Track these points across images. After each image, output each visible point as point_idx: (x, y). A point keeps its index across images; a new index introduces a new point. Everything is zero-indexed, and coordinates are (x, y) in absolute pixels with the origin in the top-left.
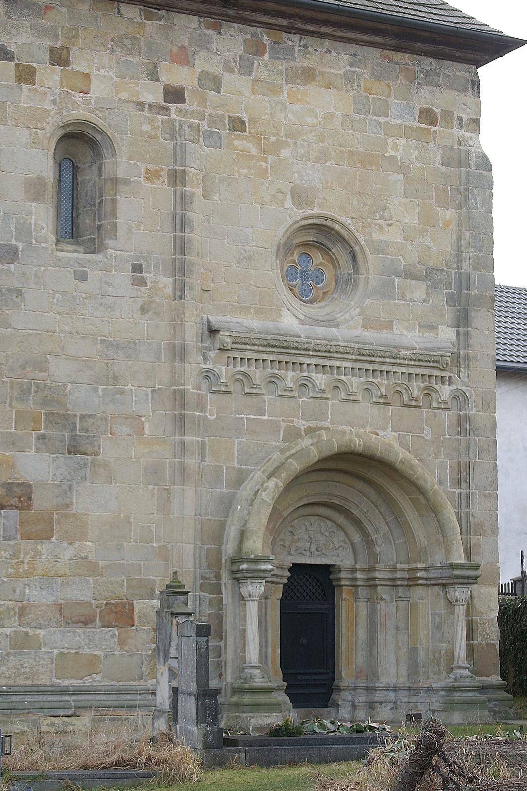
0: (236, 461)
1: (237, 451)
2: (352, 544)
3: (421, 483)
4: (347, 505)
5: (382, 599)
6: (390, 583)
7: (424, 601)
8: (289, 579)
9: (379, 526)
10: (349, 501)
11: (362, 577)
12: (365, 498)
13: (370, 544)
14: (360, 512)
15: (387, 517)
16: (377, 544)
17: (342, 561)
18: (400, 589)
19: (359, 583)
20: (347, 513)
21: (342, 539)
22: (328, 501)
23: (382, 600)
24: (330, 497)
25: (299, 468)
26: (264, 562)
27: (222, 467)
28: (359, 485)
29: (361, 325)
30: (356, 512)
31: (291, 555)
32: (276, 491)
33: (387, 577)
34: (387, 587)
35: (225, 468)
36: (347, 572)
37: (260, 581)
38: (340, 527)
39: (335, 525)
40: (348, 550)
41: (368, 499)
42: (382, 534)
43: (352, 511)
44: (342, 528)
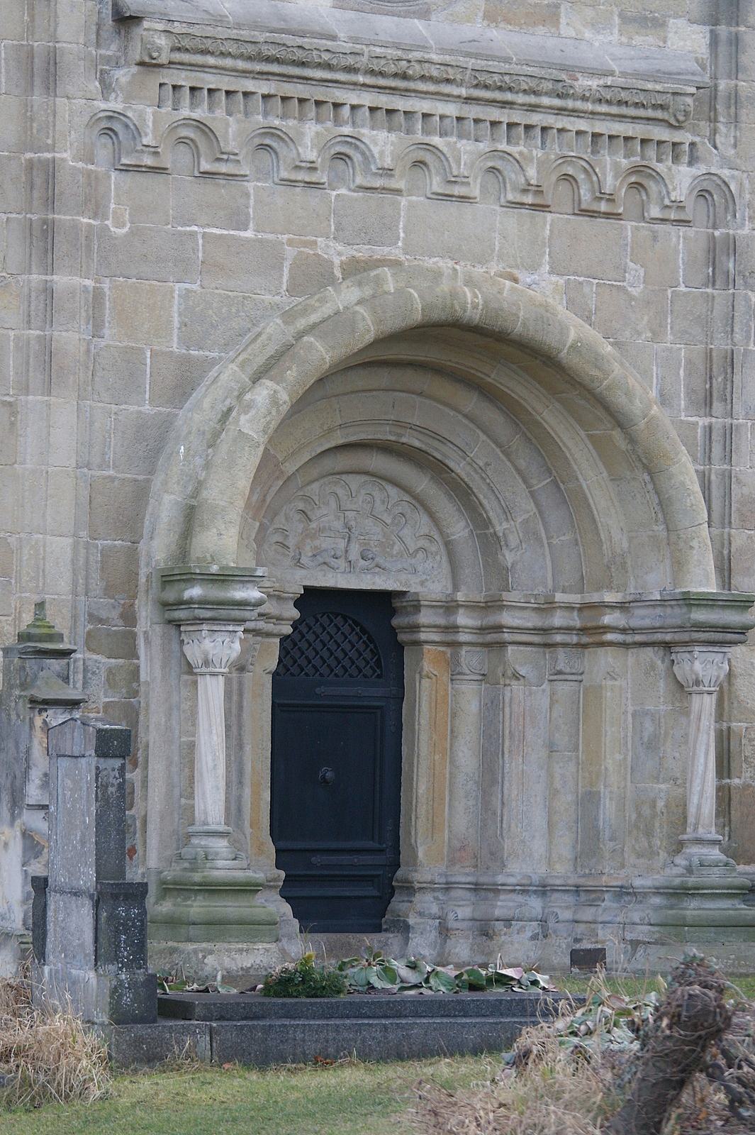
0: (175, 339)
1: (180, 315)
2: (447, 544)
4: (437, 449)
5: (516, 676)
9: (514, 504)
10: (444, 440)
13: (489, 543)
14: (468, 468)
18: (561, 652)
19: (463, 637)
21: (425, 530)
22: (393, 438)
27: (141, 351)
28: (470, 402)
29: (481, 14)
30: (460, 468)
33: (530, 625)
35: (148, 354)
37: (231, 628)
38: (420, 502)
41: (488, 436)
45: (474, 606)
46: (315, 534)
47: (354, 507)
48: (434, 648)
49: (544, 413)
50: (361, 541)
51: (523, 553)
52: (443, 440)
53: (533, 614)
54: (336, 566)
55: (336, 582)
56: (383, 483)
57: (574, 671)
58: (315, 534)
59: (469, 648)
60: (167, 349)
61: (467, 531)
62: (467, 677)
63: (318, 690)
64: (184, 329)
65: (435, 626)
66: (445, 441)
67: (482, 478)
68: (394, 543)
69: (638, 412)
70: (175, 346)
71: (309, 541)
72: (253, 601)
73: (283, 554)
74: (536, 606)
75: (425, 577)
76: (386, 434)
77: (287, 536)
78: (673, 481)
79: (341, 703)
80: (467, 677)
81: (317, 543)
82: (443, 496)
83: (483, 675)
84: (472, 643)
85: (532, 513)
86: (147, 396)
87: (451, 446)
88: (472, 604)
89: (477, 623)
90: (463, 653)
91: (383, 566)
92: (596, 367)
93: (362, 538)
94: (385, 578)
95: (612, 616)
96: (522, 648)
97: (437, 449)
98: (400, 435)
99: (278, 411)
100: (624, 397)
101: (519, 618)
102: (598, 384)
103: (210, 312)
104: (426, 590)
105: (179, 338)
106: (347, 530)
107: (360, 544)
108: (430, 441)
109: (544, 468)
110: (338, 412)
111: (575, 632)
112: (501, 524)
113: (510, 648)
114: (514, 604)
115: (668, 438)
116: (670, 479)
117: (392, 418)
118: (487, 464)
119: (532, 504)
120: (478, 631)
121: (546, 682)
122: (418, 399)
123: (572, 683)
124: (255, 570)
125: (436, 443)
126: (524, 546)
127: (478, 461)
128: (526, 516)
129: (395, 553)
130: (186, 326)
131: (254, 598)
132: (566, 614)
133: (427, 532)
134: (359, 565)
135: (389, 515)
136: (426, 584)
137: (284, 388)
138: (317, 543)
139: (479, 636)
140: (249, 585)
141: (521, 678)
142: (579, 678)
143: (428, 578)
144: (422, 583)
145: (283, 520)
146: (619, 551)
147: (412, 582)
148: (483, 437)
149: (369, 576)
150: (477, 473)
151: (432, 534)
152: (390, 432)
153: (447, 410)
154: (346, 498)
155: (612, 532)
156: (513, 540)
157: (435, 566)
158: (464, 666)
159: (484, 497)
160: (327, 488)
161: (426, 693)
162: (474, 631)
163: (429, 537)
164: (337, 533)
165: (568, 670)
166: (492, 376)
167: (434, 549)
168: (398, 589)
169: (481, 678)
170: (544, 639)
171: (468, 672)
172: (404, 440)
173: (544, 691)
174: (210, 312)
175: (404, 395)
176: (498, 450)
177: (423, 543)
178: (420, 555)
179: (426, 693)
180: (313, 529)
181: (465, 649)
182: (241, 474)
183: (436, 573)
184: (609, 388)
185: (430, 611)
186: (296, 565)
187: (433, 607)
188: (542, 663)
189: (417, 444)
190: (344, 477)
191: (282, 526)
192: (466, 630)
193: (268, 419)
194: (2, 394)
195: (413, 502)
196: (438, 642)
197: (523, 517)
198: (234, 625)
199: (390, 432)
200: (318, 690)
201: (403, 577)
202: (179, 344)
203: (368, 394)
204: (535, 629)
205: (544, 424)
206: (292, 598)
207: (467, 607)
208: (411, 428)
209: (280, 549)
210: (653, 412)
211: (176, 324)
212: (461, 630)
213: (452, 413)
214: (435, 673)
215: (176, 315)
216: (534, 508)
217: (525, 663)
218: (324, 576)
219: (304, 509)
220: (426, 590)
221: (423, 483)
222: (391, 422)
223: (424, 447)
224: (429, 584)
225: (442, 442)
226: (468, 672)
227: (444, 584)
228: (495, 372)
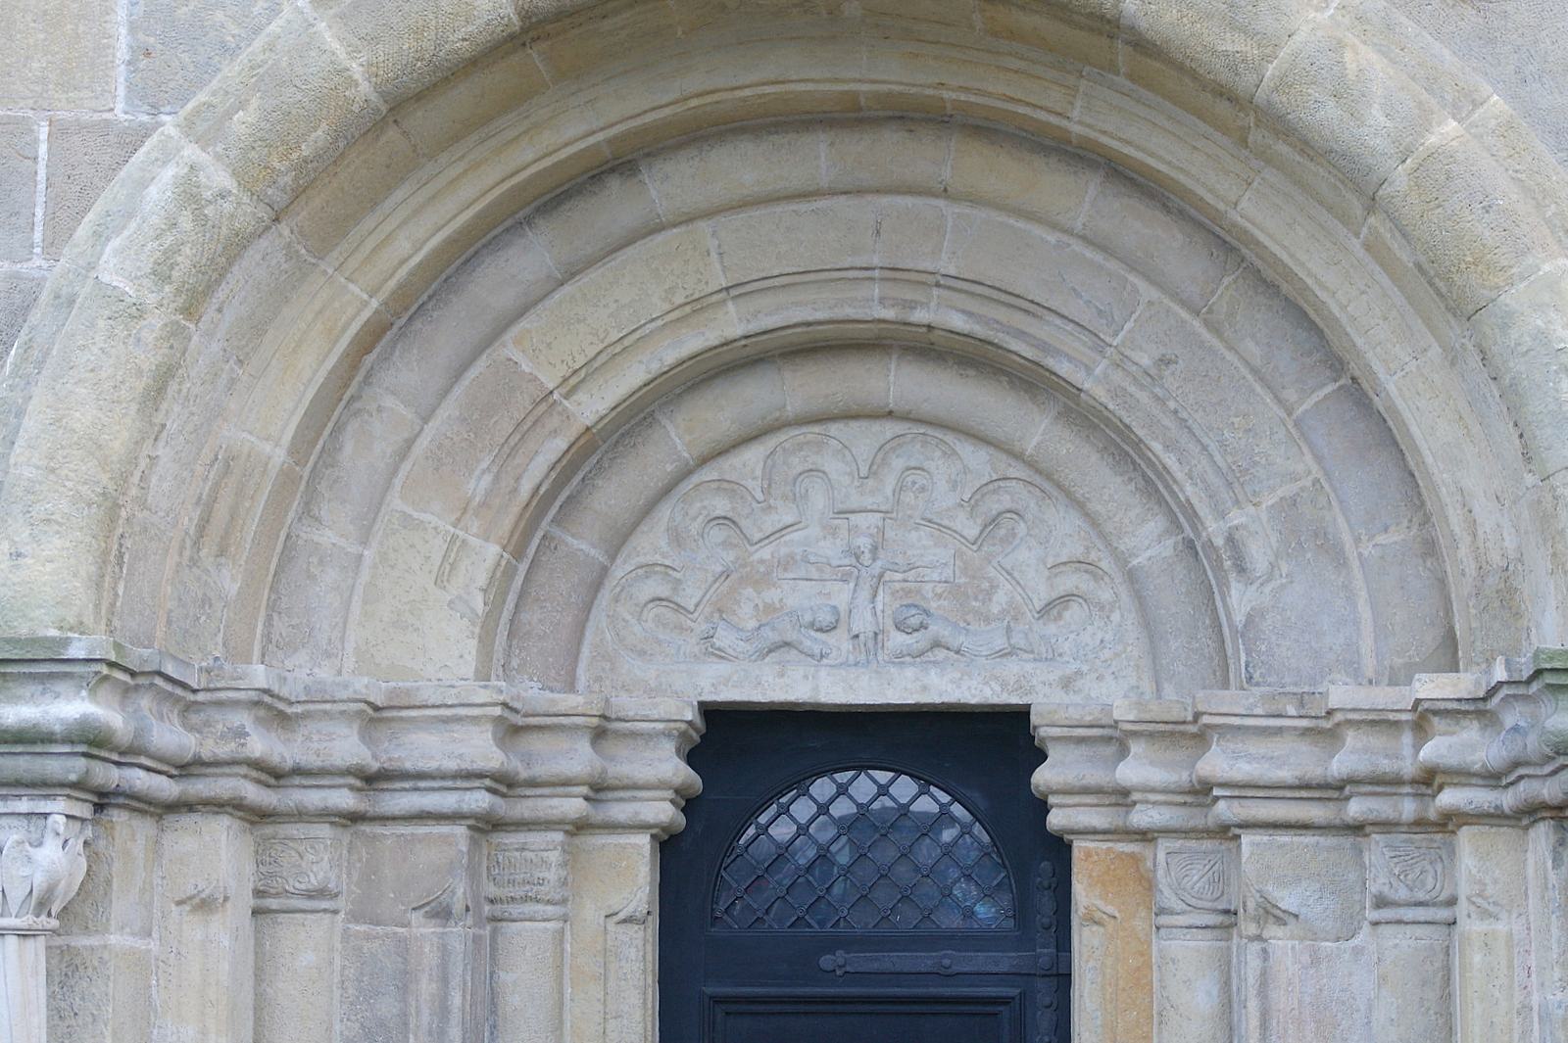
0: (121, 92)
1: (133, 28)
2: (1132, 577)
3: (1323, 114)
4: (1021, 334)
5: (1272, 913)
6: (1316, 813)
7: (1501, 927)
8: (690, 805)
9: (1253, 449)
10: (1034, 309)
11: (1157, 776)
12: (1142, 285)
13: (1205, 563)
14: (1117, 377)
15: (1291, 395)
16: (1241, 570)
17: (1067, 683)
18: (1377, 850)
19: (1143, 817)
20: (1032, 380)
21: (1074, 549)
22: (889, 314)
23: (1280, 922)
24: (908, 294)
25: (357, 71)
26: (32, 677)
27: (24, 127)
28: (1083, 200)
30: (1095, 382)
31: (721, 655)
32: (186, 222)
33: (1286, 774)
34: (1309, 839)
35: (43, 132)
36: (1084, 750)
37: (24, 806)
38: (1044, 475)
39: (1017, 470)
40: (1116, 617)
41: (1159, 286)
42: (1269, 500)
43: (1064, 369)
44: (1059, 486)
45: (1172, 733)
46: (768, 573)
47: (868, 502)
48: (1105, 846)
49: (1244, 204)
50: (898, 586)
51: (1283, 586)
52: (1032, 307)
53: (1304, 747)
55: (816, 688)
57: (1421, 896)
58: (768, 573)
59: (1178, 844)
60: (96, 117)
61: (1170, 542)
62: (1181, 920)
63: (826, 961)
64: (143, 63)
65: (1086, 791)
66: (1040, 311)
67: (1157, 398)
68: (994, 587)
69: (1379, 143)
70: (120, 106)
71: (749, 591)
72: (57, 728)
73: (681, 628)
74: (1305, 723)
75: (1073, 667)
76: (872, 305)
77: (679, 581)
78: (1514, 334)
79: (933, 991)
80: (1181, 920)
81: (772, 595)
82: (1094, 457)
83: (1227, 912)
84: (1175, 831)
85: (1307, 482)
86: (38, 236)
87: (1058, 321)
88: (1169, 727)
89: (1180, 777)
90: (1161, 856)
91: (955, 644)
92: (1233, 26)
93: (899, 576)
95: (1454, 739)
96: (1284, 838)
97: (1021, 334)
98: (912, 305)
99: (200, 219)
100: (1332, 103)
101: (1251, 758)
102: (1252, 78)
103: (219, 16)
104: (1078, 699)
105: (130, 88)
106: (853, 561)
108: (1002, 314)
109: (1317, 356)
110: (714, 255)
111: (1407, 789)
112: (1222, 515)
113: (1247, 839)
114: (1236, 721)
115: (1487, 210)
116: (1505, 328)
117: (876, 261)
118: (1164, 361)
119: (1308, 457)
120: (1189, 799)
121: (1366, 928)
122: (949, 210)
123: (1419, 930)
124: (65, 643)
125: (1019, 320)
126: (1285, 569)
127: (1136, 356)
128: (1286, 490)
129: (995, 609)
130: (148, 54)
131: (62, 721)
132: (1377, 741)
134: (889, 644)
135: (971, 515)
136: (1079, 684)
137: (218, 157)
139: (1195, 810)
140: (61, 687)
141: (1292, 920)
142: (1443, 914)
143: (1085, 668)
144: (1067, 683)
145: (663, 543)
146: (1496, 558)
148: (1148, 292)
149: (909, 672)
150: (1142, 387)
151: (1093, 556)
152: (882, 301)
153: (1037, 230)
154: (846, 480)
155: (1476, 510)
156: (1258, 554)
157: (1109, 637)
158: (1167, 892)
159: (1166, 447)
161: (1091, 964)
162: (1180, 799)
164: (828, 569)
165: (1402, 894)
166: (1075, 114)
169: (1218, 919)
170: (1331, 813)
171: (1179, 906)
172: (920, 316)
173: (1358, 952)
174: (219, 16)
175: (909, 201)
176: (1197, 324)
179: (1091, 964)
180: (762, 561)
181: (1164, 845)
182: (81, 390)
183: (1107, 654)
184: (1283, 83)
186: (707, 653)
187: (1081, 741)
188: (1352, 877)
189: (958, 322)
190: (834, 428)
191: (658, 559)
192: (1152, 797)
193: (169, 240)
196: (1105, 832)
197: (1280, 493)
198: (32, 797)
199: (882, 301)
200: (826, 961)
202: (128, 100)
203: (803, 207)
204: (1307, 787)
205: (1257, 233)
206: (667, 734)
207: (1151, 735)
208: (937, 285)
209: (669, 615)
210: (1432, 140)
211: (122, 53)
212: (1136, 796)
213: (1052, 238)
214: (1110, 909)
215: (123, 31)
216: (1315, 468)
217: (1298, 879)
219: (730, 515)
220: (1078, 699)
221: (1037, 429)
222: (877, 273)
223: (979, 330)
225: (1034, 315)
226: (1179, 906)
227: (1133, 682)
228: (1078, 103)
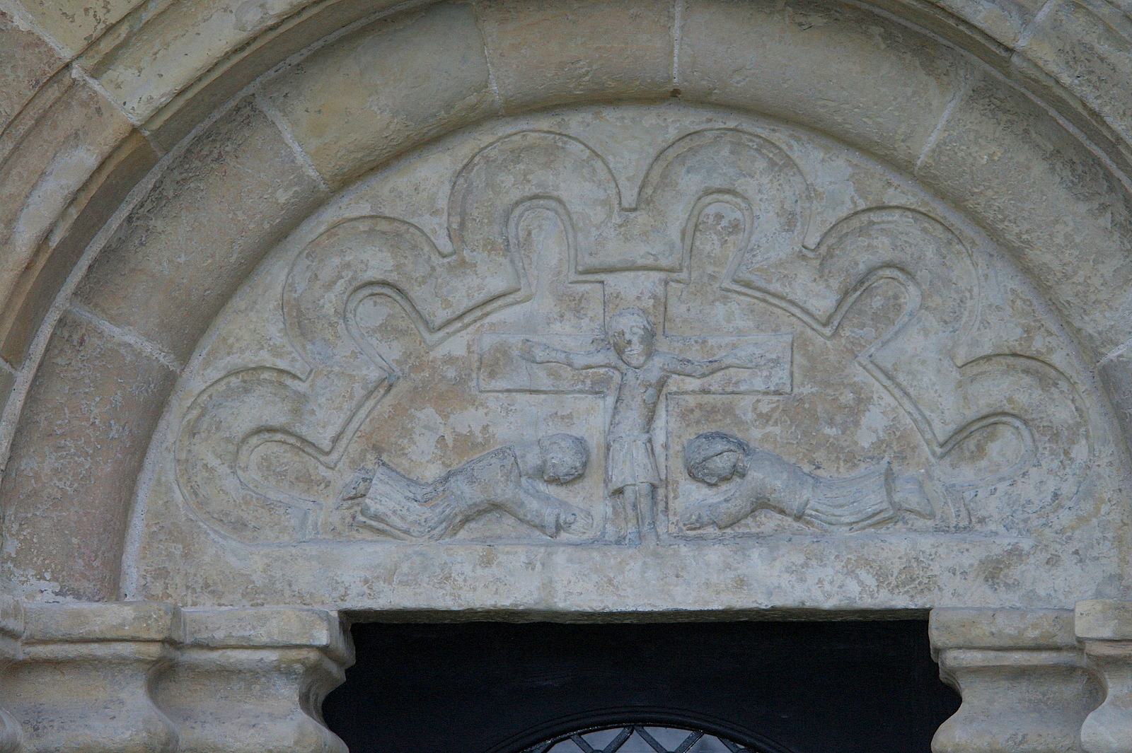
38: (951, 200)
46: (461, 381)
47: (639, 252)
50: (691, 401)
54: (549, 515)
55: (548, 585)
56: (781, 136)
58: (461, 381)
75: (1006, 541)
77: (302, 398)
81: (469, 420)
82: (1039, 168)
93: (694, 384)
94: (798, 559)
106: (612, 357)
107: (685, 414)
133: (1011, 335)
135: (822, 272)
136: (1015, 572)
138: (469, 420)
143: (1026, 544)
144: (993, 571)
145: (274, 330)
147: (936, 569)
149: (714, 554)
151: (1038, 344)
154: (598, 214)
157: (1068, 488)
160: (506, 180)
163: (1018, 358)
164: (567, 373)
167: (1062, 413)
168: (867, 602)
177: (997, 389)
178: (1006, 445)
180: (450, 360)
183: (1064, 518)
185: (1007, 696)
187: (1019, 673)
190: (576, 122)
191: (266, 358)
194: (1130, 44)
195: (940, 209)
201: (896, 546)
206: (284, 670)
218: (487, 562)
219: (393, 277)
224: (1030, 572)
227: (1113, 568)
